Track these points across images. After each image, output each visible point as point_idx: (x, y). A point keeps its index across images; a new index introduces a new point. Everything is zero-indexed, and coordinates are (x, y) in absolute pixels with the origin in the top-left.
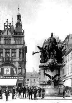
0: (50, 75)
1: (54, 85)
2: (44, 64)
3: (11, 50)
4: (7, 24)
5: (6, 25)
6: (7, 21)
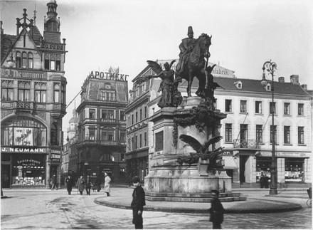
0: (197, 139)
1: (206, 167)
2: (173, 109)
3: (33, 83)
4: (25, 21)
5: (22, 22)
6: (25, 15)
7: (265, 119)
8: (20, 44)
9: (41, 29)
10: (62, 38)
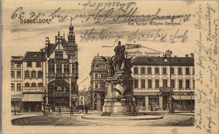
6: (59, 34)
7: (146, 77)
8: (57, 48)
9: (67, 40)
10: (76, 44)
